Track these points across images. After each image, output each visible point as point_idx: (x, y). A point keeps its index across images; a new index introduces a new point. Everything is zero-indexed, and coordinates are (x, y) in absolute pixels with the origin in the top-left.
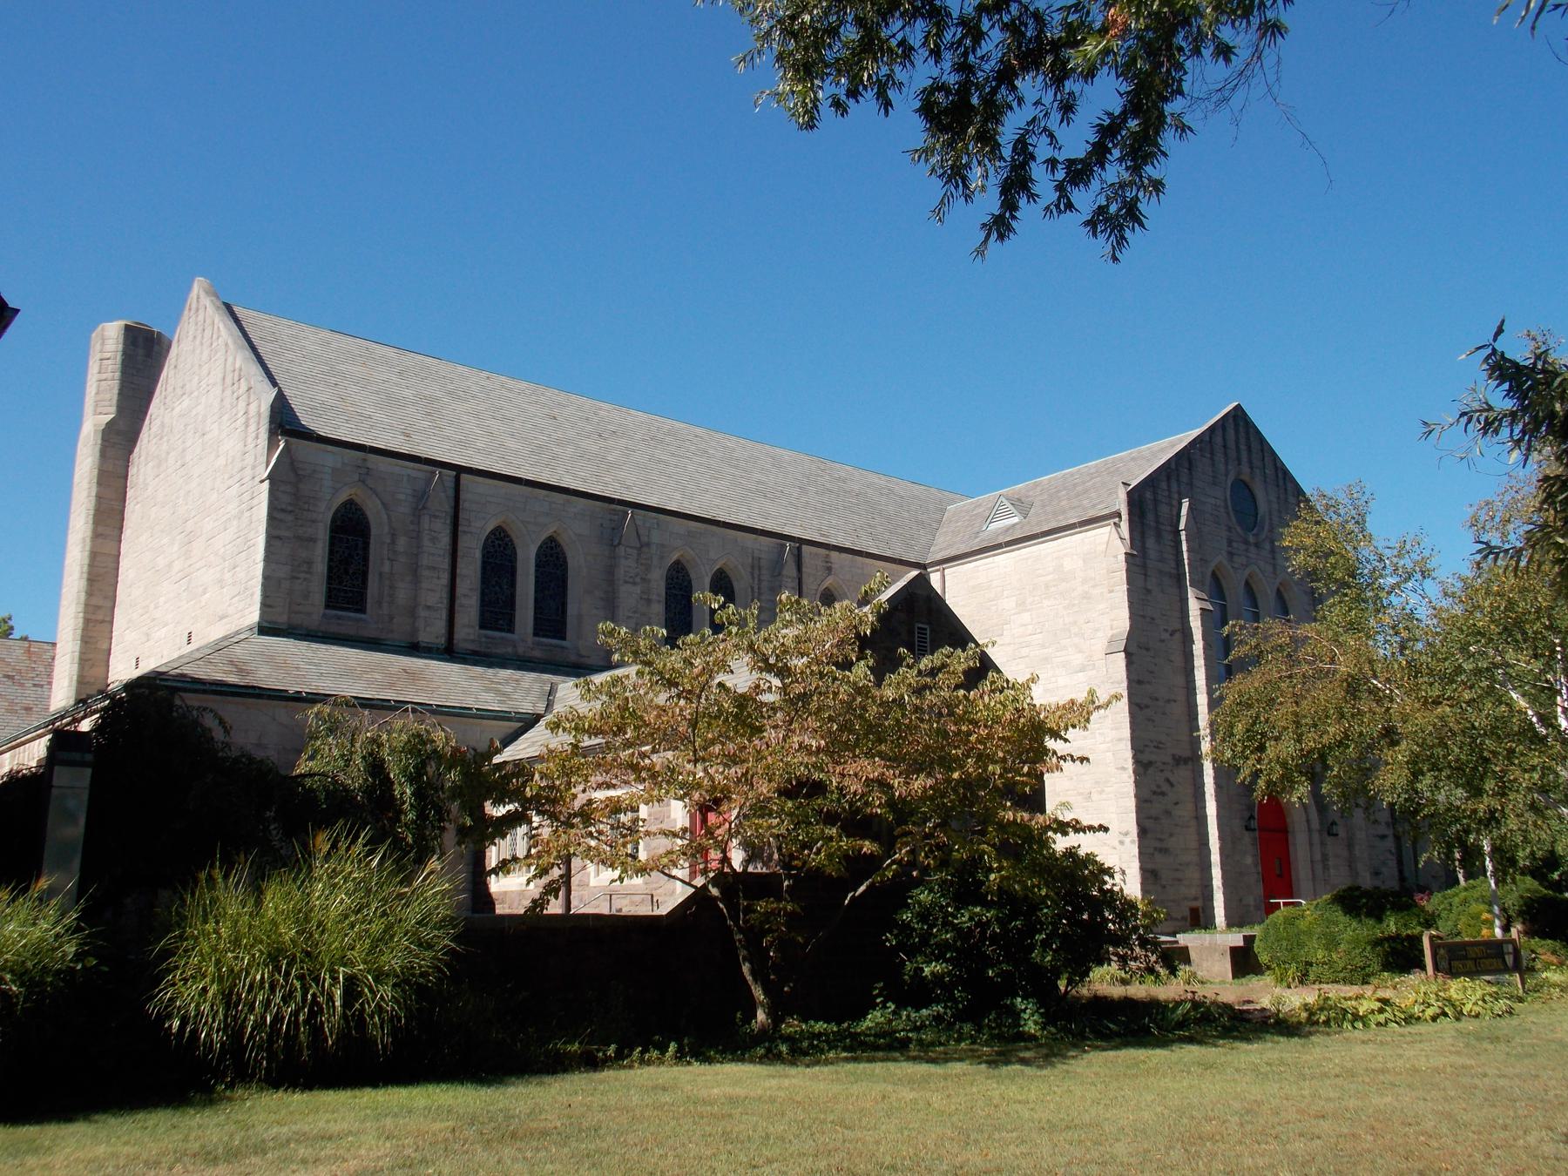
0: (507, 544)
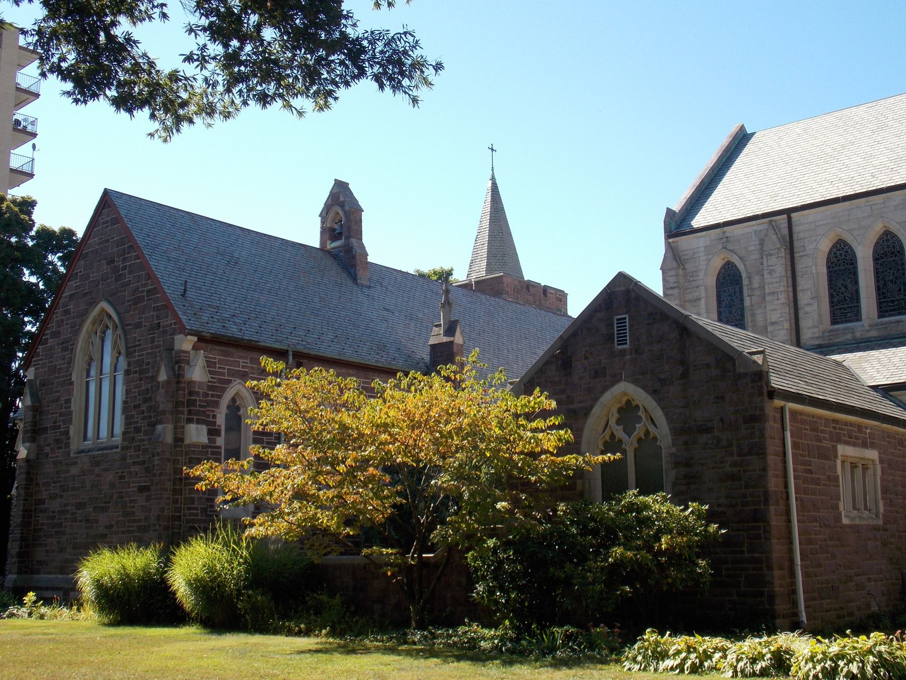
0: (847, 252)
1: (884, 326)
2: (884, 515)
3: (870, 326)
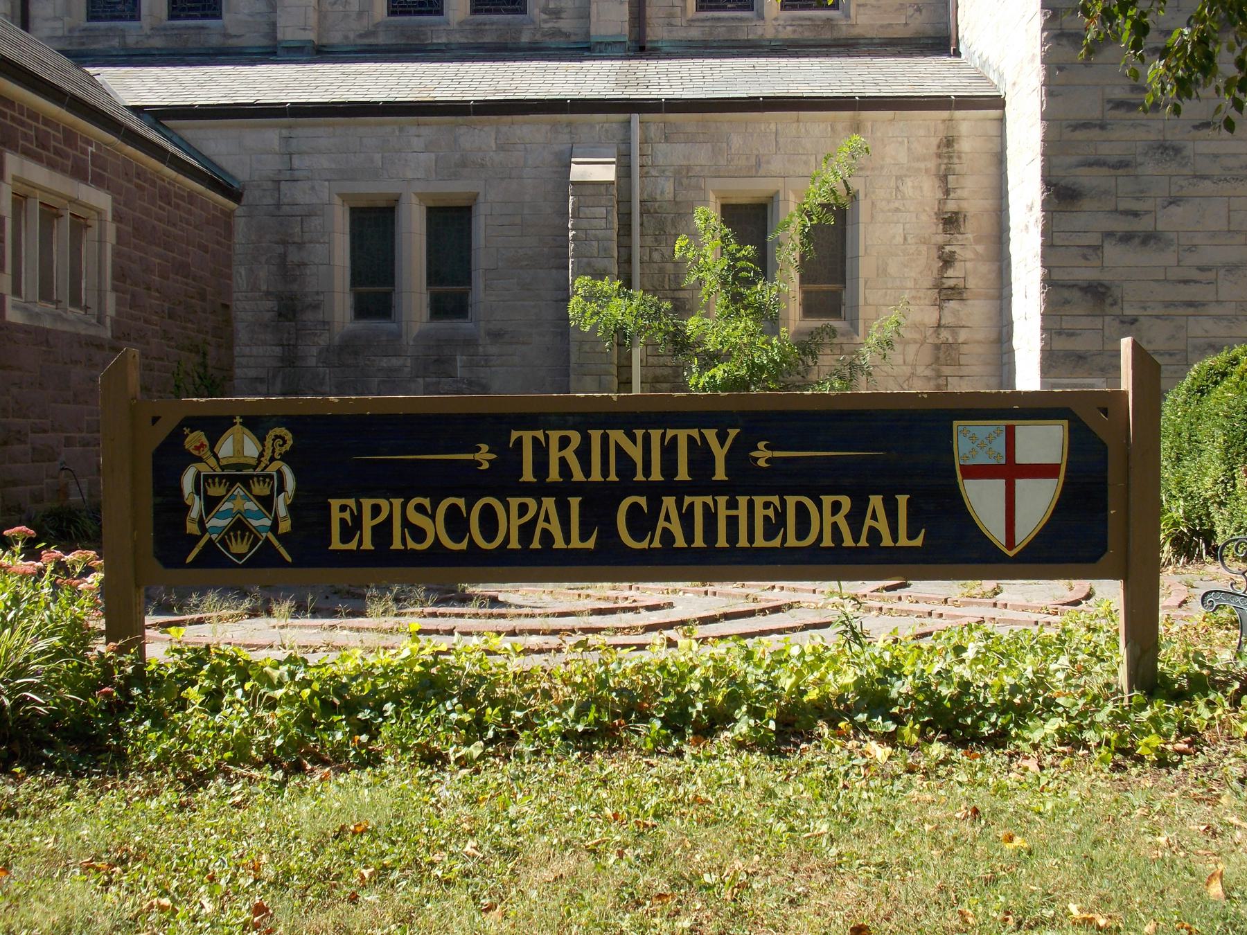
1: (176, 32)
2: (115, 322)
3: (152, 29)
